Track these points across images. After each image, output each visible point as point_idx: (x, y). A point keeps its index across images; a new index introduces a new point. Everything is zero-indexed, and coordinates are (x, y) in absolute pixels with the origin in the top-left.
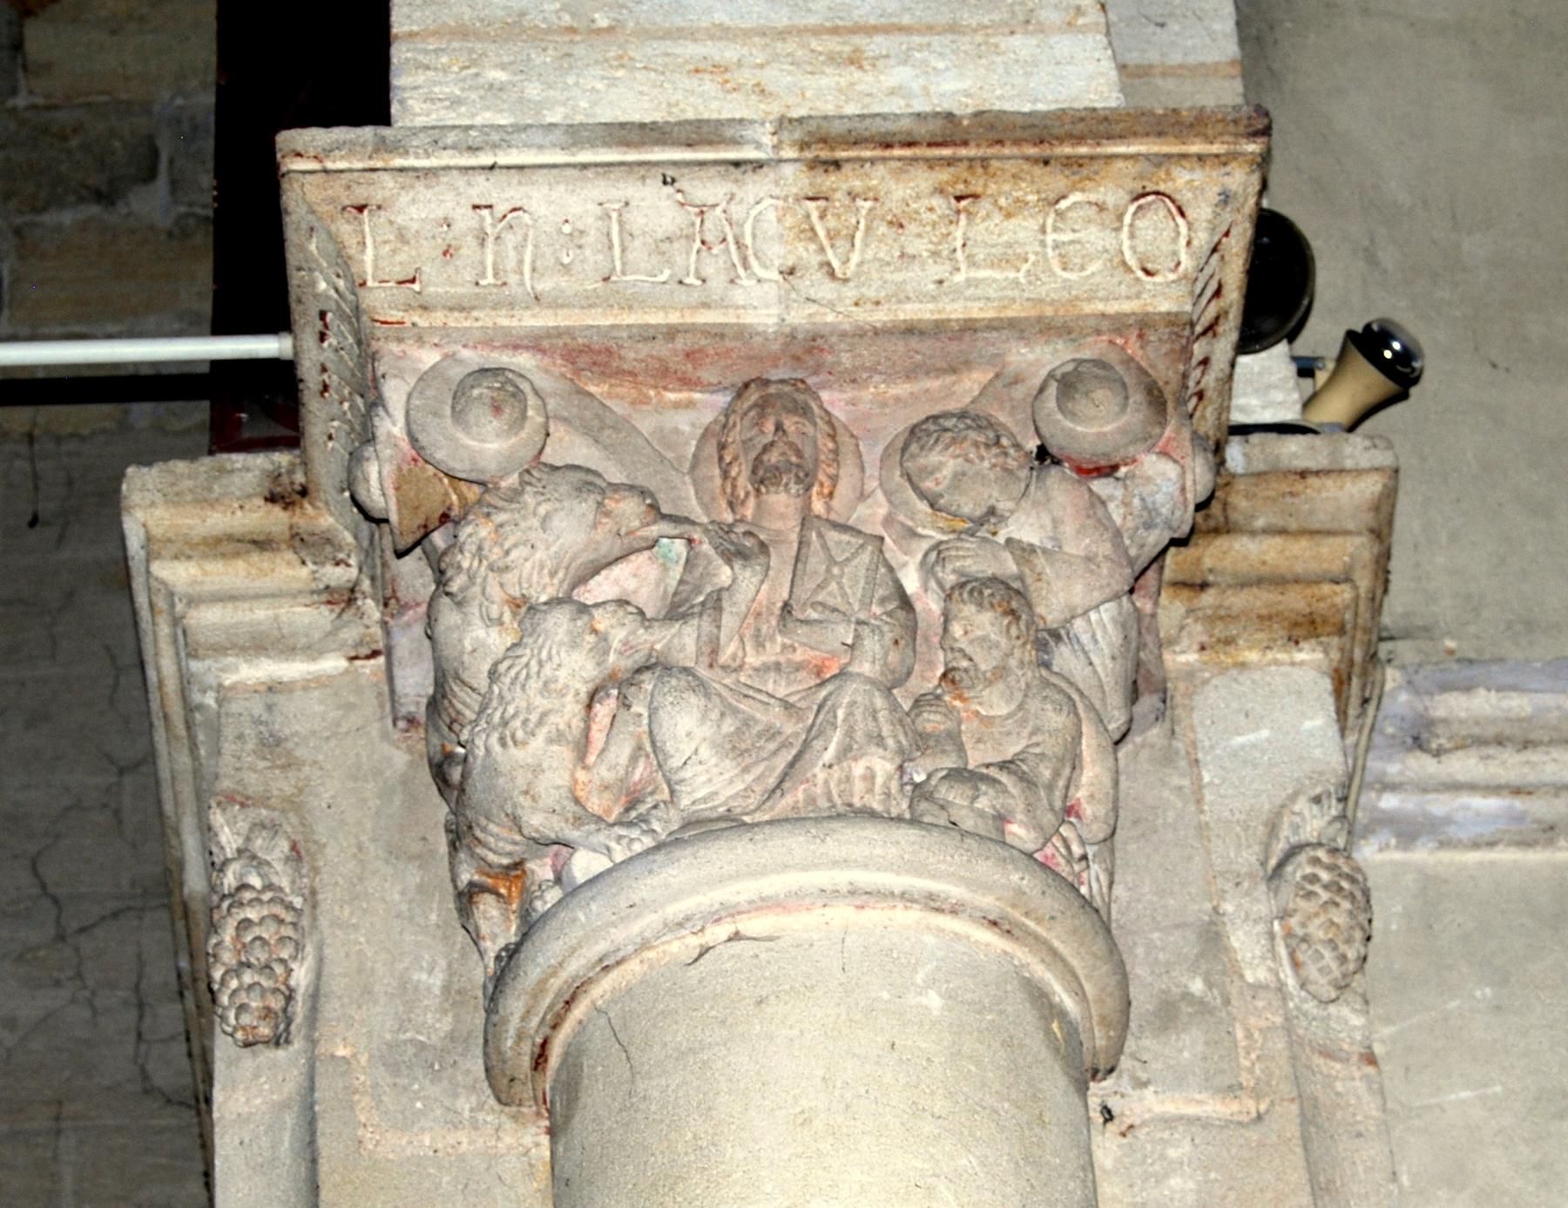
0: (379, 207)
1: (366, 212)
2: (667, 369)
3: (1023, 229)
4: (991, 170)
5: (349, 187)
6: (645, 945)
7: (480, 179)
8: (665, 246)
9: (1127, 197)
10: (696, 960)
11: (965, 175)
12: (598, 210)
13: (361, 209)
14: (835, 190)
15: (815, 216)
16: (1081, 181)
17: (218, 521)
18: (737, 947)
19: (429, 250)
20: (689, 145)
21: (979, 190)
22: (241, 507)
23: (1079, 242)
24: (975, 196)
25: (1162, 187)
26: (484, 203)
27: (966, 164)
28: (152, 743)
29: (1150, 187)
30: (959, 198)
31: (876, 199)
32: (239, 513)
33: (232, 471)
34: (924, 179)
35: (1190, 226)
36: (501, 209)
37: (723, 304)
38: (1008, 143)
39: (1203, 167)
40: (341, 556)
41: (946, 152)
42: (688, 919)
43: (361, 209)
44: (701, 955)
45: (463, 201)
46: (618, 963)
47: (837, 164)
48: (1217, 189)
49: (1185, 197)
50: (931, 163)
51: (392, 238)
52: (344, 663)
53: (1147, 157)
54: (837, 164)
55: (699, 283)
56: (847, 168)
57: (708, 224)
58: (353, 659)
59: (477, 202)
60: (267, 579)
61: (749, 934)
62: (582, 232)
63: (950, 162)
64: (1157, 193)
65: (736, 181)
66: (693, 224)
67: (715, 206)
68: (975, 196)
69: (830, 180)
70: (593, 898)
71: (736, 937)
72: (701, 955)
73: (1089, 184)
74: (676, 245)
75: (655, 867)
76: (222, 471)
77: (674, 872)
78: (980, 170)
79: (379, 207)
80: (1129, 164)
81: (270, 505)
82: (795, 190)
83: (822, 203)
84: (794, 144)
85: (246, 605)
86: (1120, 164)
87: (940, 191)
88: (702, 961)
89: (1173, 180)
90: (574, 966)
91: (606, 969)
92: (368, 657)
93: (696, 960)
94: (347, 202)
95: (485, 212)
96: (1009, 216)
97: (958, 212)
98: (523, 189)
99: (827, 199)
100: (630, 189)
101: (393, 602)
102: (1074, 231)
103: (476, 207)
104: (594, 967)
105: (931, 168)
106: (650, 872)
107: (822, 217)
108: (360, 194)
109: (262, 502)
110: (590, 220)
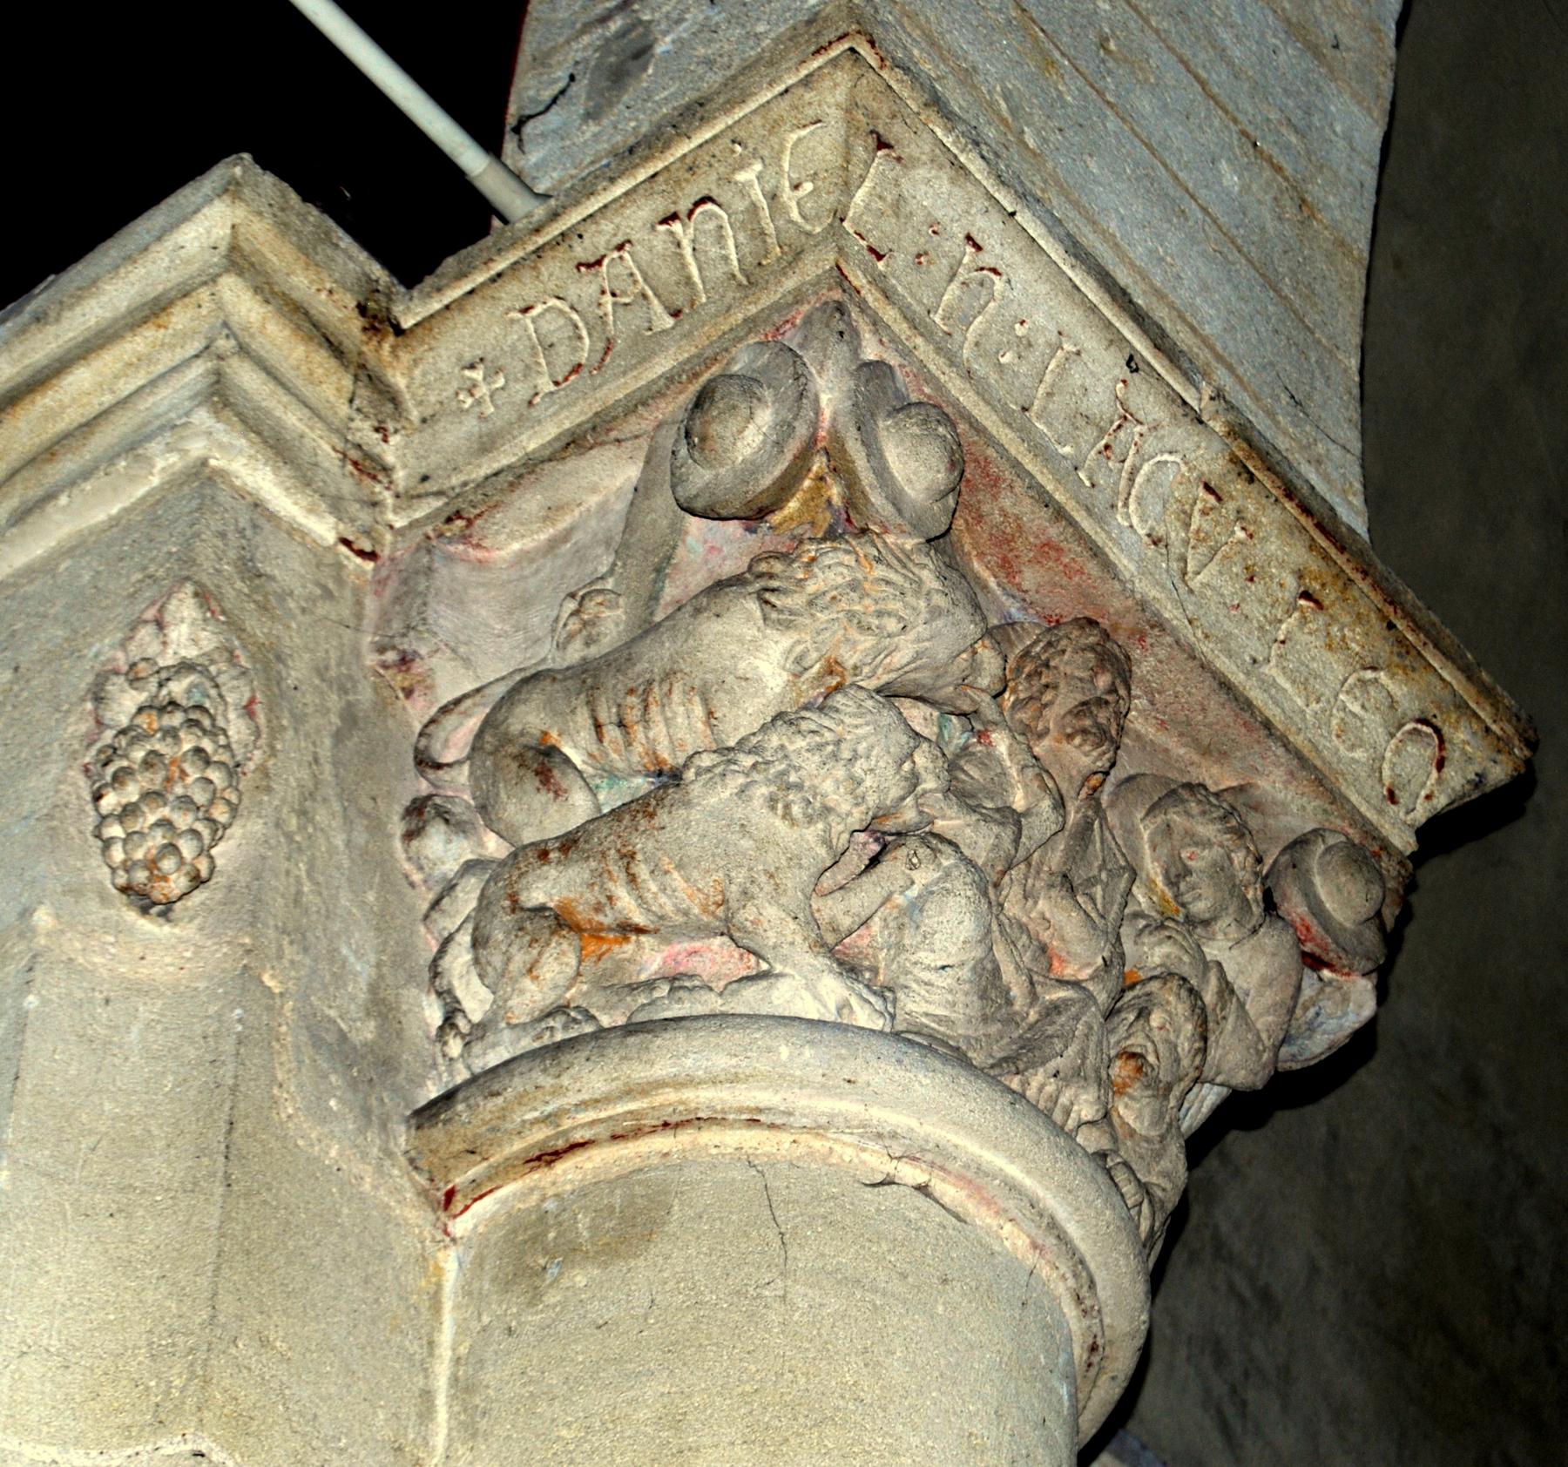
0: (899, 159)
1: (884, 151)
2: (1008, 542)
3: (1334, 668)
4: (1348, 594)
5: (894, 116)
6: (818, 1130)
7: (995, 216)
8: (1081, 422)
9: (1417, 715)
10: (874, 1185)
11: (1329, 579)
12: (1054, 338)
13: (882, 144)
14: (1232, 497)
15: (1199, 505)
16: (1397, 666)
17: (301, 282)
18: (920, 1200)
19: (910, 242)
20: (1156, 346)
21: (1326, 603)
22: (331, 292)
23: (1362, 720)
24: (1319, 605)
25: (1446, 730)
26: (979, 241)
27: (1335, 571)
28: (241, 493)
29: (1438, 722)
30: (1306, 595)
31: (1251, 536)
32: (323, 296)
33: (337, 246)
34: (1299, 554)
35: (1440, 781)
36: (987, 259)
37: (1100, 521)
38: (1369, 580)
39: (1484, 738)
40: (390, 426)
41: (1322, 542)
42: (894, 1136)
43: (882, 144)
44: (882, 1184)
45: (964, 221)
46: (772, 1126)
47: (1251, 479)
48: (1478, 769)
49: (1454, 755)
50: (1313, 546)
51: (889, 199)
52: (331, 538)
53: (1454, 693)
54: (1251, 479)
55: (1087, 483)
56: (1255, 487)
57: (1122, 434)
58: (346, 542)
59: (974, 235)
60: (310, 388)
61: (937, 1195)
62: (1030, 345)
63: (1326, 557)
64: (1437, 731)
65: (1174, 416)
66: (1112, 422)
67: (1139, 422)
68: (1319, 605)
69: (1238, 487)
70: (811, 1043)
71: (923, 1189)
72: (882, 1184)
73: (1400, 675)
74: (1089, 430)
75: (906, 1061)
76: (328, 237)
77: (926, 1081)
78: (1340, 583)
79: (899, 159)
80: (1439, 685)
81: (356, 313)
82: (1205, 468)
83: (1212, 500)
84: (1228, 423)
85: (286, 399)
86: (1435, 680)
87: (1300, 575)
88: (882, 1190)
89: (1456, 729)
90: (702, 1098)
91: (754, 1122)
92: (361, 553)
93: (874, 1185)
94: (881, 130)
95: (970, 249)
96: (1329, 647)
97: (1295, 609)
98: (1017, 258)
99: (1219, 499)
100: (1092, 342)
101: (460, 523)
102: (1363, 707)
103: (969, 238)
104: (740, 1111)
105: (1311, 548)
106: (899, 1062)
107: (1204, 513)
108: (895, 131)
109: (353, 304)
110: (1041, 341)
